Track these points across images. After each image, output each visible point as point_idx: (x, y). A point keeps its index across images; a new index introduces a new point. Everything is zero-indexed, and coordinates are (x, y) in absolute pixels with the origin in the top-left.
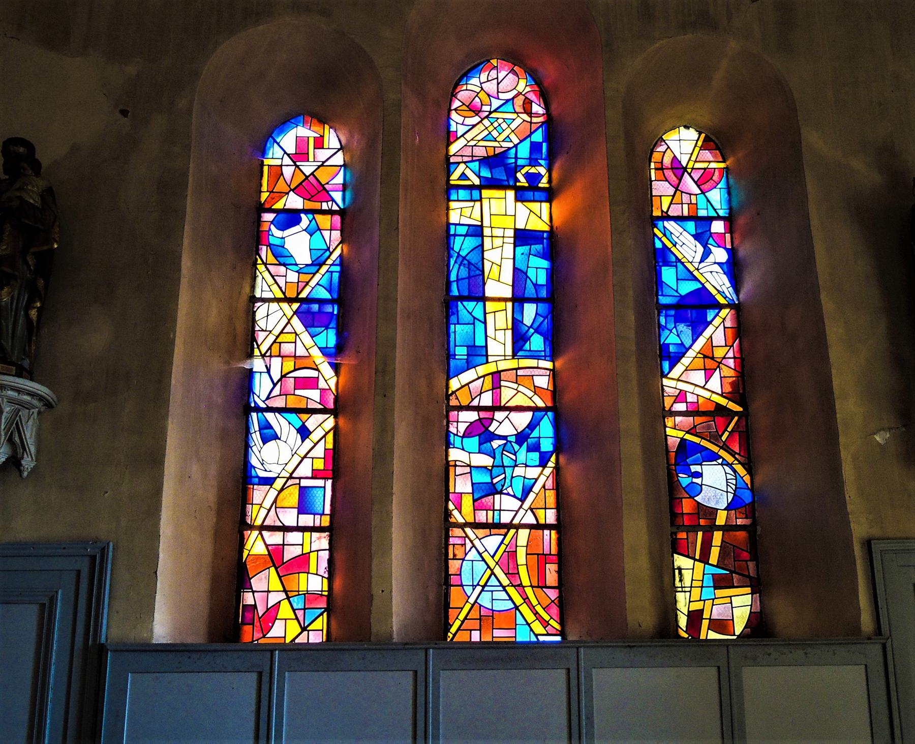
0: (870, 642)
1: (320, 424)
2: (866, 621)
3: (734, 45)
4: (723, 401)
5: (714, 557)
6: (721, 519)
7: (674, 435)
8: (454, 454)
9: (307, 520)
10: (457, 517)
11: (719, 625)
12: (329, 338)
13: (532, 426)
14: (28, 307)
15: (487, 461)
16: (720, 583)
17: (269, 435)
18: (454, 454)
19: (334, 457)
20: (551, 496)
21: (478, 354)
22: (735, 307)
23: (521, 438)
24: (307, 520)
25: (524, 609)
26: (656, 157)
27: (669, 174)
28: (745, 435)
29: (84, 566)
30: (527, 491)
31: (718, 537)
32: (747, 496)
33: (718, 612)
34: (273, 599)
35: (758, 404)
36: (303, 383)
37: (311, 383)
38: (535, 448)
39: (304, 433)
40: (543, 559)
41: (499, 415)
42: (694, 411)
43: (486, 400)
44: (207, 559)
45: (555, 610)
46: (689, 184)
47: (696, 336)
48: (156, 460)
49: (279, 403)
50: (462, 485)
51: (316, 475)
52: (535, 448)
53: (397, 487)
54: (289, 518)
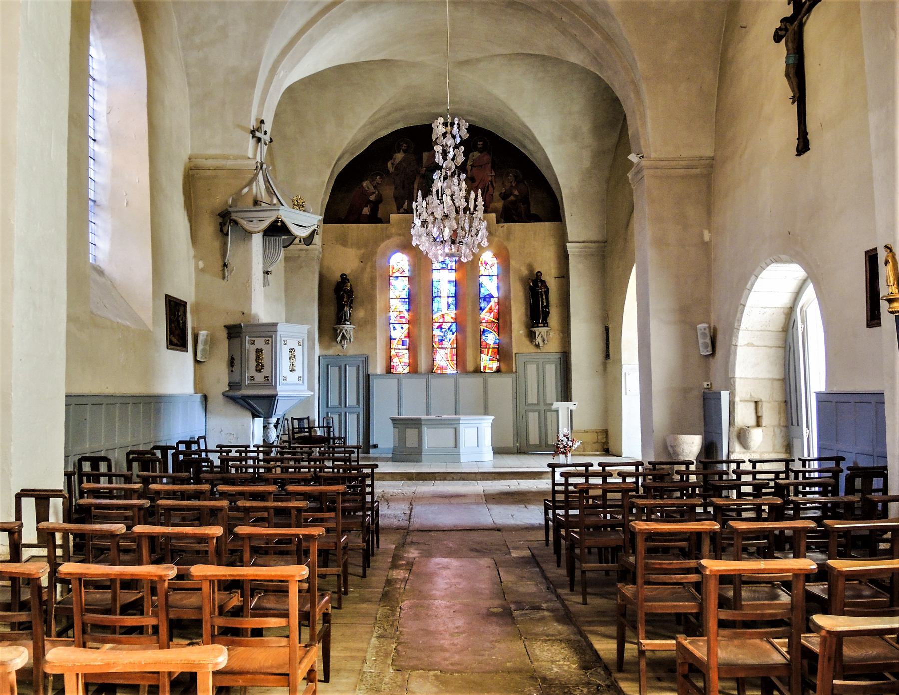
0: (802, 322)
1: (406, 326)
2: (514, 370)
3: (496, 239)
4: (494, 320)
5: (490, 354)
6: (492, 346)
7: (482, 328)
8: (434, 333)
9: (403, 347)
10: (435, 346)
11: (490, 369)
12: (406, 307)
13: (451, 326)
14: (350, 310)
15: (441, 334)
16: (491, 360)
17: (394, 329)
18: (434, 333)
19: (408, 333)
20: (455, 342)
21: (439, 309)
22: (498, 298)
23: (449, 329)
24: (403, 347)
25: (449, 365)
26: (481, 260)
27: (484, 264)
28: (498, 328)
29: (364, 360)
30: (450, 340)
31: (491, 350)
32: (498, 341)
33: (491, 366)
34: (397, 364)
35: (501, 321)
36: (401, 317)
37: (403, 317)
38: (452, 331)
39: (402, 328)
40: (453, 355)
41: (444, 324)
42: (487, 322)
43: (441, 320)
44: (385, 356)
45: (456, 366)
46: (488, 267)
47: (488, 304)
48: (375, 338)
49: (396, 322)
50: (436, 340)
51: (405, 337)
52: (452, 331)
53: (422, 342)
54: (400, 347)
